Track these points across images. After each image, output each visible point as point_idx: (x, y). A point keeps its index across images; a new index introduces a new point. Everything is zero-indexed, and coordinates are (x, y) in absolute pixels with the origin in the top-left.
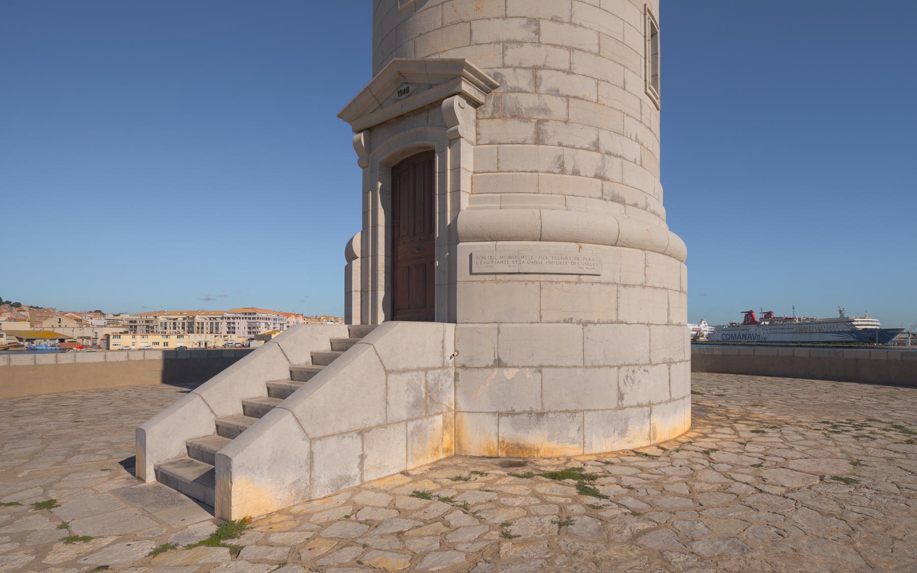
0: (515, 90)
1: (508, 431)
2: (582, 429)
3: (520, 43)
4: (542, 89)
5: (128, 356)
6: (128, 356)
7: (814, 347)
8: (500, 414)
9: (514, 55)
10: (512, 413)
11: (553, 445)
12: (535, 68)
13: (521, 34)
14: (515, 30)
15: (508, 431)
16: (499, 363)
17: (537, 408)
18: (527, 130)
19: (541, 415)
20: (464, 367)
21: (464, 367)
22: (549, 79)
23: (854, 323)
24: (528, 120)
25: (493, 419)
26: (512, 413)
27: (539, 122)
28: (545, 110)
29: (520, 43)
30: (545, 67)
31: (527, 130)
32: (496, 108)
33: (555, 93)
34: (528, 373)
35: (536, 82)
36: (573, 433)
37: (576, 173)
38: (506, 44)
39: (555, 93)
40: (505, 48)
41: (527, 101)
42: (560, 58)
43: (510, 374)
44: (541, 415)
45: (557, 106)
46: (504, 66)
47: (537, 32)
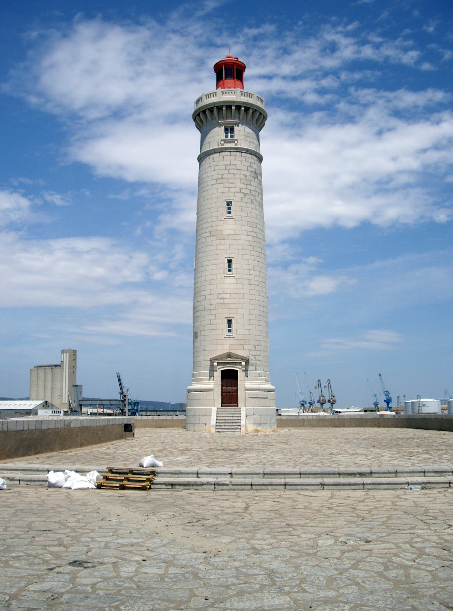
1: (255, 427)
15: (255, 427)
16: (254, 414)
33: (258, 360)
38: (250, 350)
39: (258, 360)
41: (254, 362)
43: (256, 416)
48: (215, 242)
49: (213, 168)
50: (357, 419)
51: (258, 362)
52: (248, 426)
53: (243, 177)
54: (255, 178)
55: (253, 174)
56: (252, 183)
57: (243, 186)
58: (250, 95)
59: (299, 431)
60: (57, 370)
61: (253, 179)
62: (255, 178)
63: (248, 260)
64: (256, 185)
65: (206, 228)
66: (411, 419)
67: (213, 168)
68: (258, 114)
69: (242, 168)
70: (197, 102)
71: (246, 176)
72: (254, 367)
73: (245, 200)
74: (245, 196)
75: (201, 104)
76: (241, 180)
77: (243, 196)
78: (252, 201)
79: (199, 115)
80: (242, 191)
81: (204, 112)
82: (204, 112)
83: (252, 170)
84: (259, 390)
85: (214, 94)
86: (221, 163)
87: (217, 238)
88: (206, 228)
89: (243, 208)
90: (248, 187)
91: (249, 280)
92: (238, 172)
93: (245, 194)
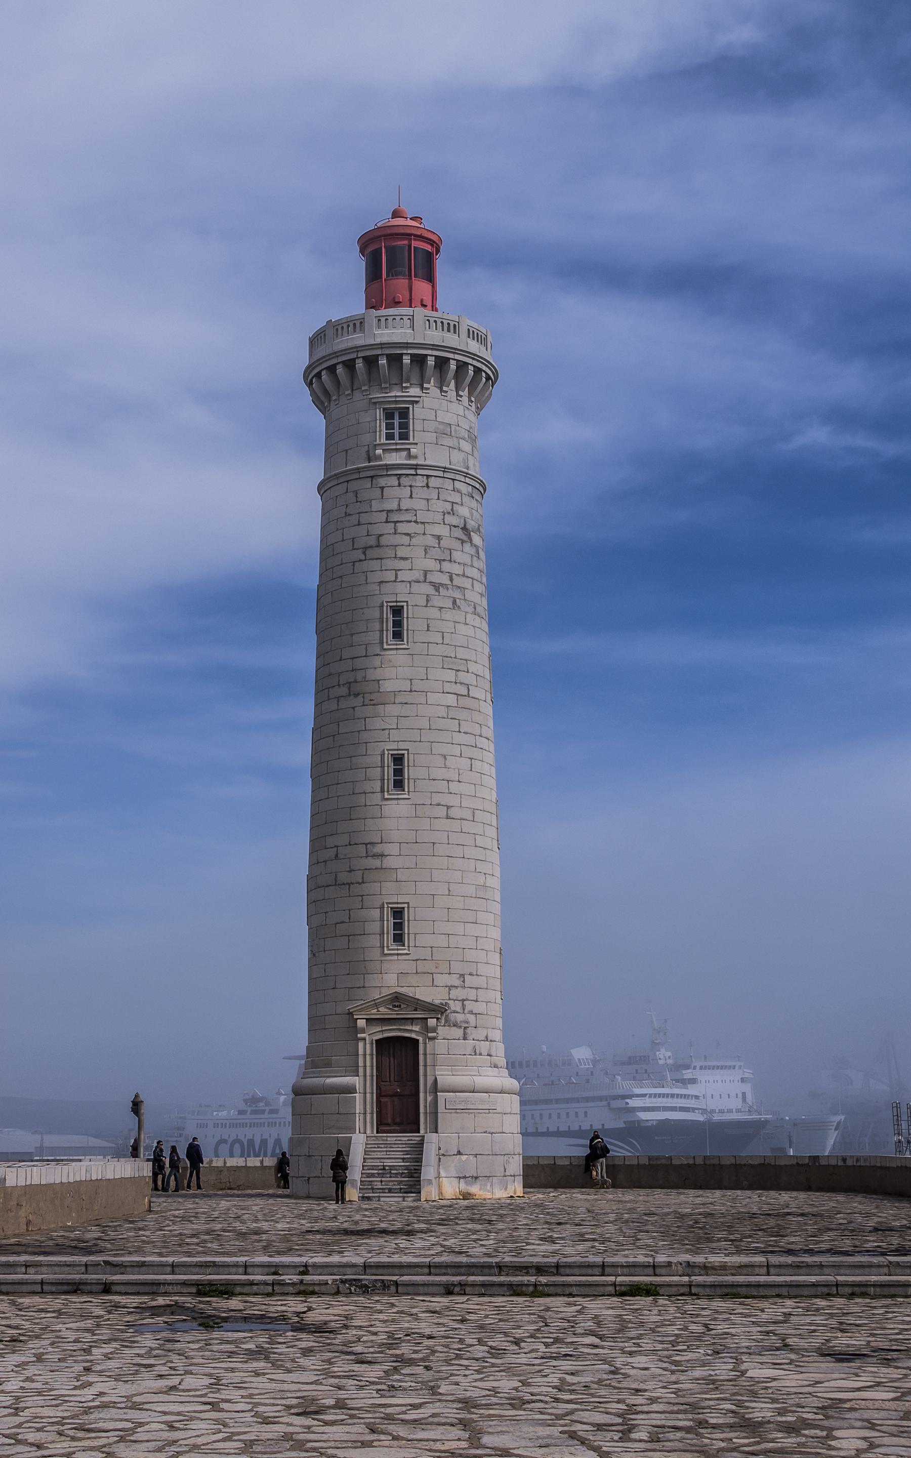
0: (455, 1012)
1: (463, 1186)
2: (492, 1185)
3: (456, 987)
4: (466, 1011)
5: (42, 1139)
6: (42, 1139)
7: (607, 1413)
8: (460, 1178)
9: (454, 993)
10: (465, 1177)
11: (481, 1193)
12: (463, 1000)
13: (457, 982)
14: (454, 980)
15: (463, 1186)
16: (459, 1153)
17: (475, 1175)
18: (459, 1033)
19: (476, 1178)
20: (443, 1155)
21: (443, 1155)
22: (469, 1005)
23: (633, 1103)
24: (460, 1027)
25: (456, 1180)
26: (465, 1177)
27: (465, 1028)
28: (467, 1022)
29: (456, 987)
30: (467, 1000)
31: (459, 1033)
32: (446, 1021)
33: (471, 1012)
34: (471, 1157)
35: (464, 1007)
36: (489, 1188)
37: (480, 1054)
38: (450, 987)
39: (471, 1012)
40: (450, 990)
41: (460, 1017)
42: (472, 994)
43: (464, 1158)
44: (476, 1178)
45: (472, 1018)
46: (450, 999)
47: (464, 982)
48: (359, 712)
49: (354, 520)
50: (752, 1166)
51: (472, 1018)
52: (445, 1182)
53: (432, 542)
54: (463, 542)
55: (458, 533)
56: (457, 556)
57: (431, 564)
58: (453, 328)
59: (579, 1196)
60: (531, 1129)
61: (457, 545)
62: (463, 542)
63: (445, 757)
64: (467, 560)
65: (340, 674)
66: (881, 1168)
67: (354, 520)
68: (471, 373)
69: (429, 517)
70: (317, 340)
71: (439, 538)
72: (461, 1031)
73: (437, 601)
74: (437, 590)
75: (321, 352)
76: (426, 549)
77: (431, 590)
78: (454, 602)
79: (318, 375)
80: (430, 578)
81: (332, 369)
82: (332, 369)
83: (454, 520)
84: (674, 1109)
85: (357, 324)
86: (376, 506)
87: (367, 702)
88: (340, 674)
89: (432, 623)
90: (447, 566)
91: (448, 807)
92: (419, 528)
93: (437, 587)
